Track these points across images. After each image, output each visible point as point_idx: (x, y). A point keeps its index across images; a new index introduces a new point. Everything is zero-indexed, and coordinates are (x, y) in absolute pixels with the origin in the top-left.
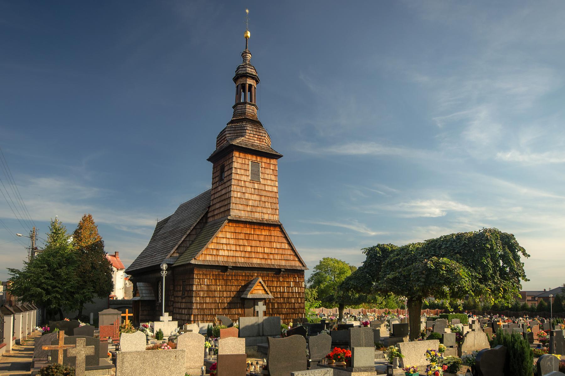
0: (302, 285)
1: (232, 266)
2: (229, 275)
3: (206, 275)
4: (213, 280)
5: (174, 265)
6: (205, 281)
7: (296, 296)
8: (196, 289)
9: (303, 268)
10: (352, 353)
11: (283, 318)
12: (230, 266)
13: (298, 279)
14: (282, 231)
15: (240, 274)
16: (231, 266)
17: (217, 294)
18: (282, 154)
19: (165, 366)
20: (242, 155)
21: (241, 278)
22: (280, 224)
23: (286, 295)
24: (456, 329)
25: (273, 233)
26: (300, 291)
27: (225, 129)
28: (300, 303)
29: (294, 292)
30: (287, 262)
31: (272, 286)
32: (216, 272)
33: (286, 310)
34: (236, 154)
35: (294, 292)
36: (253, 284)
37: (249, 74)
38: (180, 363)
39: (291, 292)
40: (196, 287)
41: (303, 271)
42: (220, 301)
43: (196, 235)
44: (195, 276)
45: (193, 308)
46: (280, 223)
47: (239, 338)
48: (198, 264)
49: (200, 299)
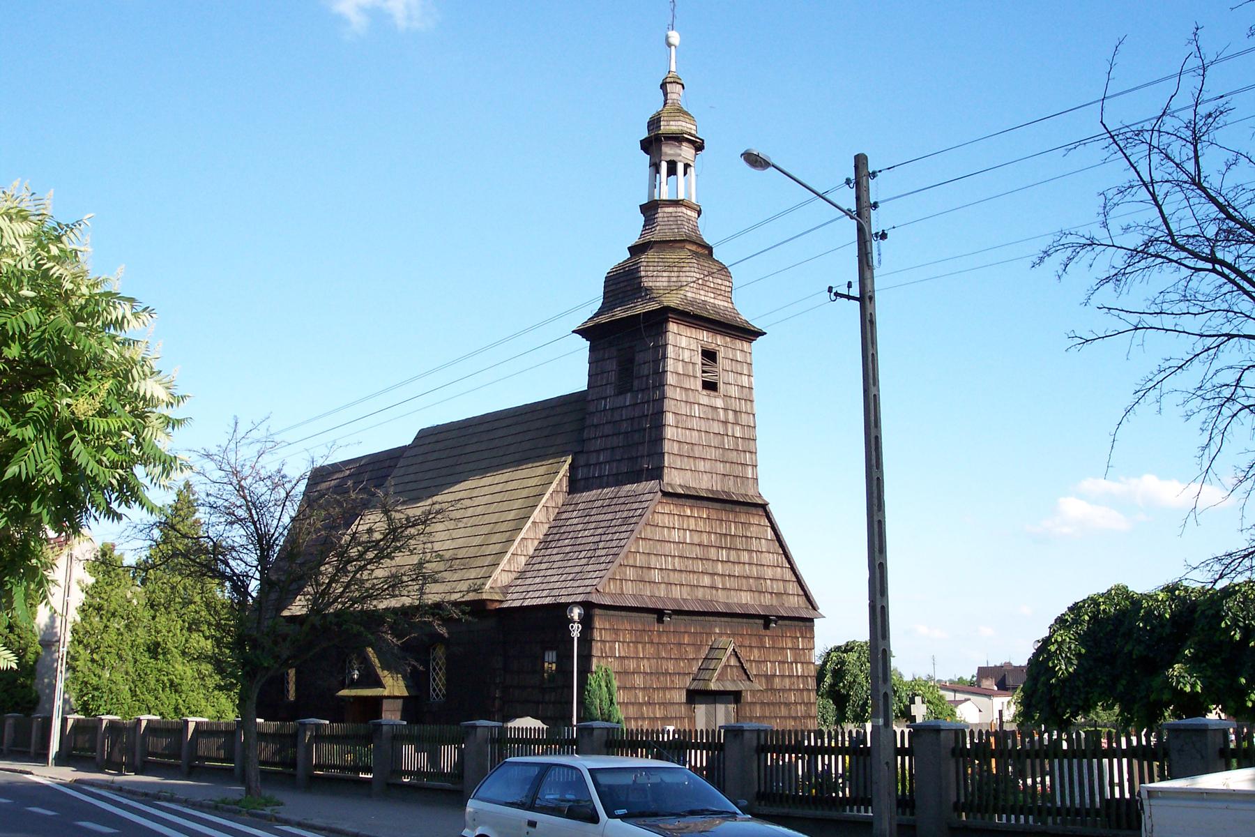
2: (663, 631)
4: (631, 644)
6: (615, 648)
17: (639, 681)
22: (763, 503)
25: (754, 520)
30: (691, 576)
33: (778, 721)
34: (673, 327)
41: (811, 620)
42: (646, 699)
46: (763, 500)
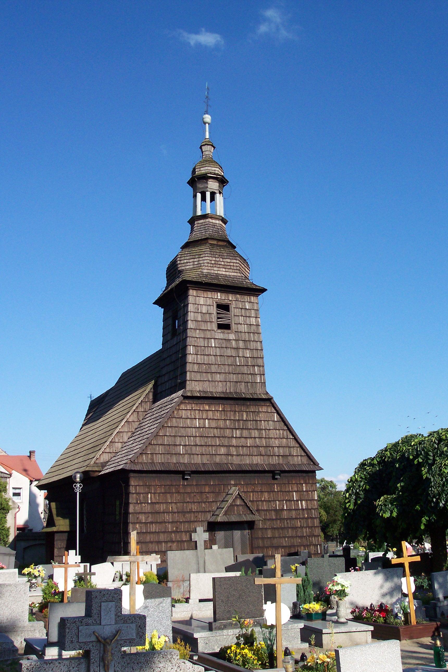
0: (312, 496)
5: (102, 473)
7: (303, 515)
8: (134, 510)
10: (404, 617)
12: (187, 471)
13: (306, 487)
14: (274, 406)
16: (189, 471)
19: (4, 603)
20: (201, 293)
21: (207, 489)
23: (285, 514)
27: (177, 256)
28: (312, 527)
29: (300, 508)
32: (167, 480)
35: (300, 508)
38: (22, 600)
39: (295, 510)
40: (134, 507)
44: (132, 490)
48: (153, 470)
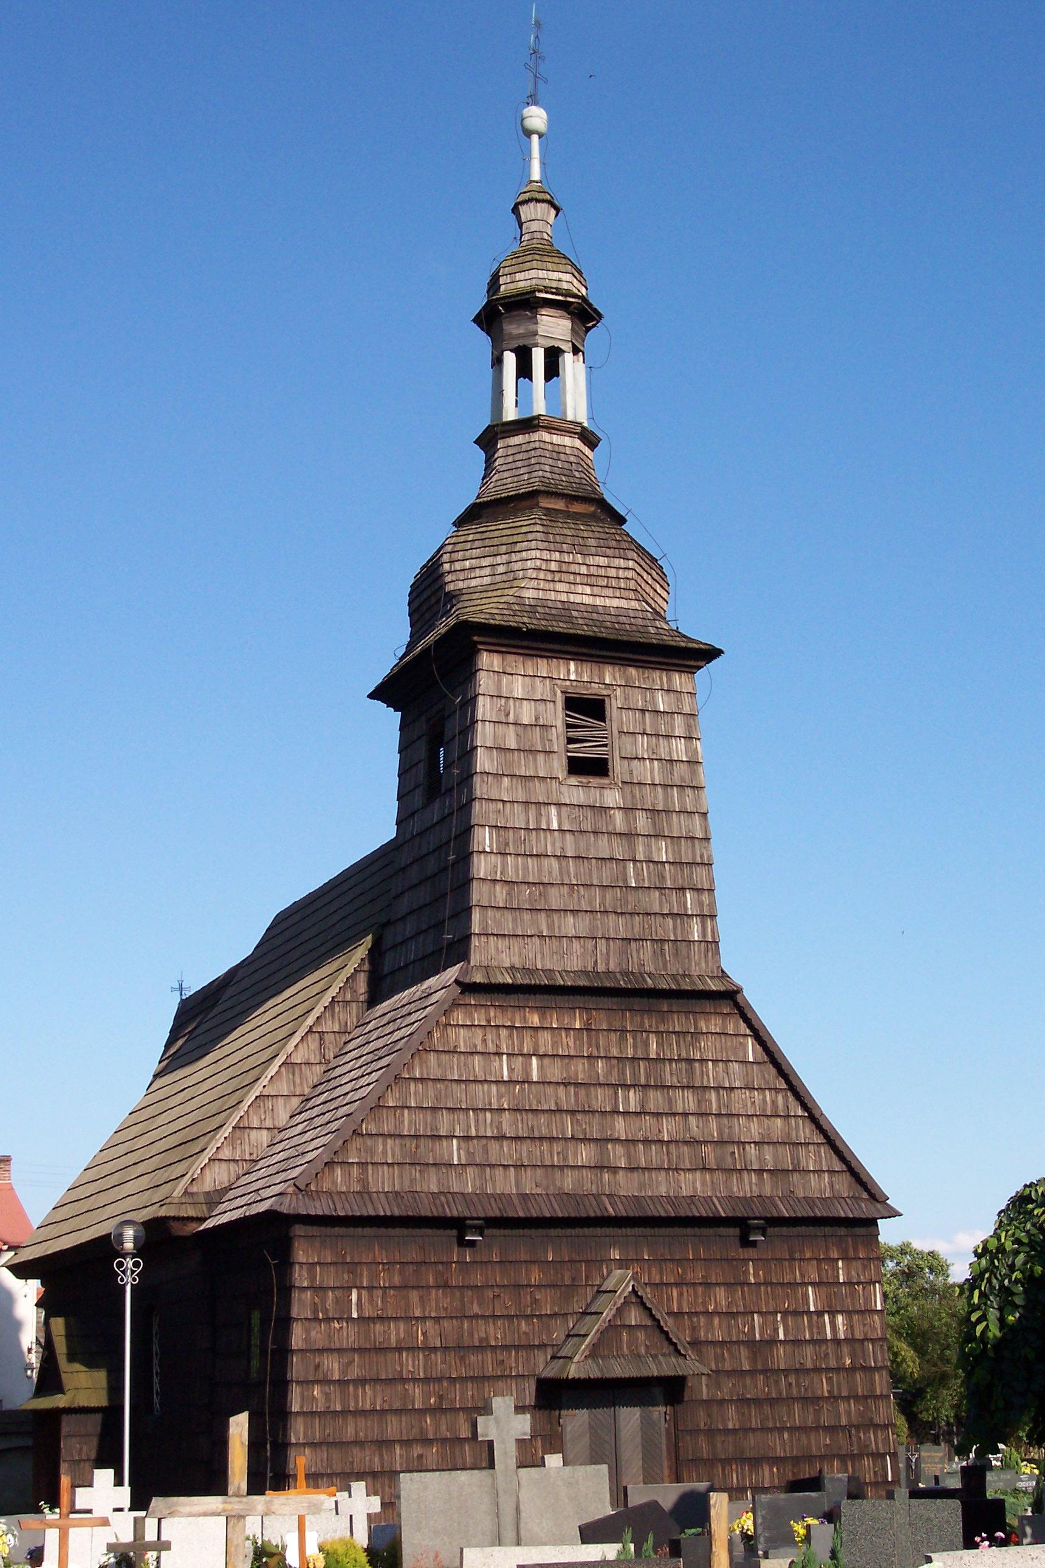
1: (482, 1214)
3: (353, 1267)
7: (839, 1358)
9: (865, 1210)
11: (776, 1481)
13: (847, 1269)
14: (744, 1014)
15: (621, 1239)
16: (478, 1219)
18: (902, 1213)
24: (538, 1046)
26: (858, 1335)
29: (829, 1337)
31: (706, 1313)
35: (829, 1337)
36: (596, 1313)
37: (546, 290)
39: (813, 1341)
40: (307, 1331)
43: (324, 1068)
45: (293, 1440)
47: (584, 1546)
49: (327, 1395)
